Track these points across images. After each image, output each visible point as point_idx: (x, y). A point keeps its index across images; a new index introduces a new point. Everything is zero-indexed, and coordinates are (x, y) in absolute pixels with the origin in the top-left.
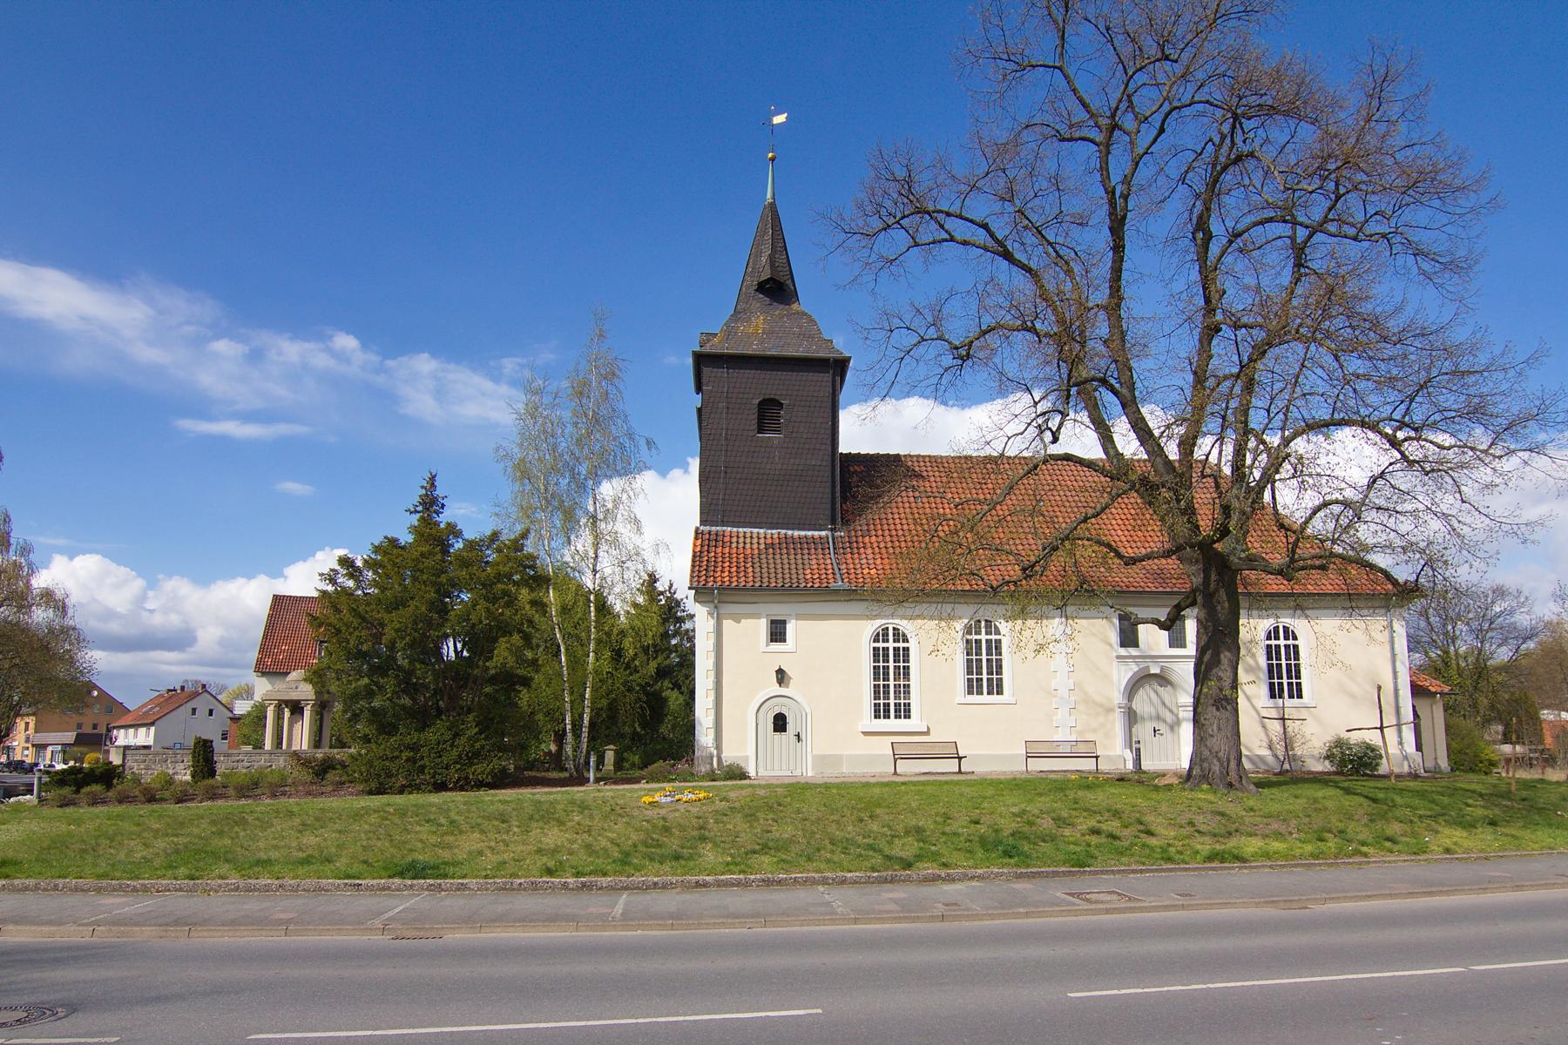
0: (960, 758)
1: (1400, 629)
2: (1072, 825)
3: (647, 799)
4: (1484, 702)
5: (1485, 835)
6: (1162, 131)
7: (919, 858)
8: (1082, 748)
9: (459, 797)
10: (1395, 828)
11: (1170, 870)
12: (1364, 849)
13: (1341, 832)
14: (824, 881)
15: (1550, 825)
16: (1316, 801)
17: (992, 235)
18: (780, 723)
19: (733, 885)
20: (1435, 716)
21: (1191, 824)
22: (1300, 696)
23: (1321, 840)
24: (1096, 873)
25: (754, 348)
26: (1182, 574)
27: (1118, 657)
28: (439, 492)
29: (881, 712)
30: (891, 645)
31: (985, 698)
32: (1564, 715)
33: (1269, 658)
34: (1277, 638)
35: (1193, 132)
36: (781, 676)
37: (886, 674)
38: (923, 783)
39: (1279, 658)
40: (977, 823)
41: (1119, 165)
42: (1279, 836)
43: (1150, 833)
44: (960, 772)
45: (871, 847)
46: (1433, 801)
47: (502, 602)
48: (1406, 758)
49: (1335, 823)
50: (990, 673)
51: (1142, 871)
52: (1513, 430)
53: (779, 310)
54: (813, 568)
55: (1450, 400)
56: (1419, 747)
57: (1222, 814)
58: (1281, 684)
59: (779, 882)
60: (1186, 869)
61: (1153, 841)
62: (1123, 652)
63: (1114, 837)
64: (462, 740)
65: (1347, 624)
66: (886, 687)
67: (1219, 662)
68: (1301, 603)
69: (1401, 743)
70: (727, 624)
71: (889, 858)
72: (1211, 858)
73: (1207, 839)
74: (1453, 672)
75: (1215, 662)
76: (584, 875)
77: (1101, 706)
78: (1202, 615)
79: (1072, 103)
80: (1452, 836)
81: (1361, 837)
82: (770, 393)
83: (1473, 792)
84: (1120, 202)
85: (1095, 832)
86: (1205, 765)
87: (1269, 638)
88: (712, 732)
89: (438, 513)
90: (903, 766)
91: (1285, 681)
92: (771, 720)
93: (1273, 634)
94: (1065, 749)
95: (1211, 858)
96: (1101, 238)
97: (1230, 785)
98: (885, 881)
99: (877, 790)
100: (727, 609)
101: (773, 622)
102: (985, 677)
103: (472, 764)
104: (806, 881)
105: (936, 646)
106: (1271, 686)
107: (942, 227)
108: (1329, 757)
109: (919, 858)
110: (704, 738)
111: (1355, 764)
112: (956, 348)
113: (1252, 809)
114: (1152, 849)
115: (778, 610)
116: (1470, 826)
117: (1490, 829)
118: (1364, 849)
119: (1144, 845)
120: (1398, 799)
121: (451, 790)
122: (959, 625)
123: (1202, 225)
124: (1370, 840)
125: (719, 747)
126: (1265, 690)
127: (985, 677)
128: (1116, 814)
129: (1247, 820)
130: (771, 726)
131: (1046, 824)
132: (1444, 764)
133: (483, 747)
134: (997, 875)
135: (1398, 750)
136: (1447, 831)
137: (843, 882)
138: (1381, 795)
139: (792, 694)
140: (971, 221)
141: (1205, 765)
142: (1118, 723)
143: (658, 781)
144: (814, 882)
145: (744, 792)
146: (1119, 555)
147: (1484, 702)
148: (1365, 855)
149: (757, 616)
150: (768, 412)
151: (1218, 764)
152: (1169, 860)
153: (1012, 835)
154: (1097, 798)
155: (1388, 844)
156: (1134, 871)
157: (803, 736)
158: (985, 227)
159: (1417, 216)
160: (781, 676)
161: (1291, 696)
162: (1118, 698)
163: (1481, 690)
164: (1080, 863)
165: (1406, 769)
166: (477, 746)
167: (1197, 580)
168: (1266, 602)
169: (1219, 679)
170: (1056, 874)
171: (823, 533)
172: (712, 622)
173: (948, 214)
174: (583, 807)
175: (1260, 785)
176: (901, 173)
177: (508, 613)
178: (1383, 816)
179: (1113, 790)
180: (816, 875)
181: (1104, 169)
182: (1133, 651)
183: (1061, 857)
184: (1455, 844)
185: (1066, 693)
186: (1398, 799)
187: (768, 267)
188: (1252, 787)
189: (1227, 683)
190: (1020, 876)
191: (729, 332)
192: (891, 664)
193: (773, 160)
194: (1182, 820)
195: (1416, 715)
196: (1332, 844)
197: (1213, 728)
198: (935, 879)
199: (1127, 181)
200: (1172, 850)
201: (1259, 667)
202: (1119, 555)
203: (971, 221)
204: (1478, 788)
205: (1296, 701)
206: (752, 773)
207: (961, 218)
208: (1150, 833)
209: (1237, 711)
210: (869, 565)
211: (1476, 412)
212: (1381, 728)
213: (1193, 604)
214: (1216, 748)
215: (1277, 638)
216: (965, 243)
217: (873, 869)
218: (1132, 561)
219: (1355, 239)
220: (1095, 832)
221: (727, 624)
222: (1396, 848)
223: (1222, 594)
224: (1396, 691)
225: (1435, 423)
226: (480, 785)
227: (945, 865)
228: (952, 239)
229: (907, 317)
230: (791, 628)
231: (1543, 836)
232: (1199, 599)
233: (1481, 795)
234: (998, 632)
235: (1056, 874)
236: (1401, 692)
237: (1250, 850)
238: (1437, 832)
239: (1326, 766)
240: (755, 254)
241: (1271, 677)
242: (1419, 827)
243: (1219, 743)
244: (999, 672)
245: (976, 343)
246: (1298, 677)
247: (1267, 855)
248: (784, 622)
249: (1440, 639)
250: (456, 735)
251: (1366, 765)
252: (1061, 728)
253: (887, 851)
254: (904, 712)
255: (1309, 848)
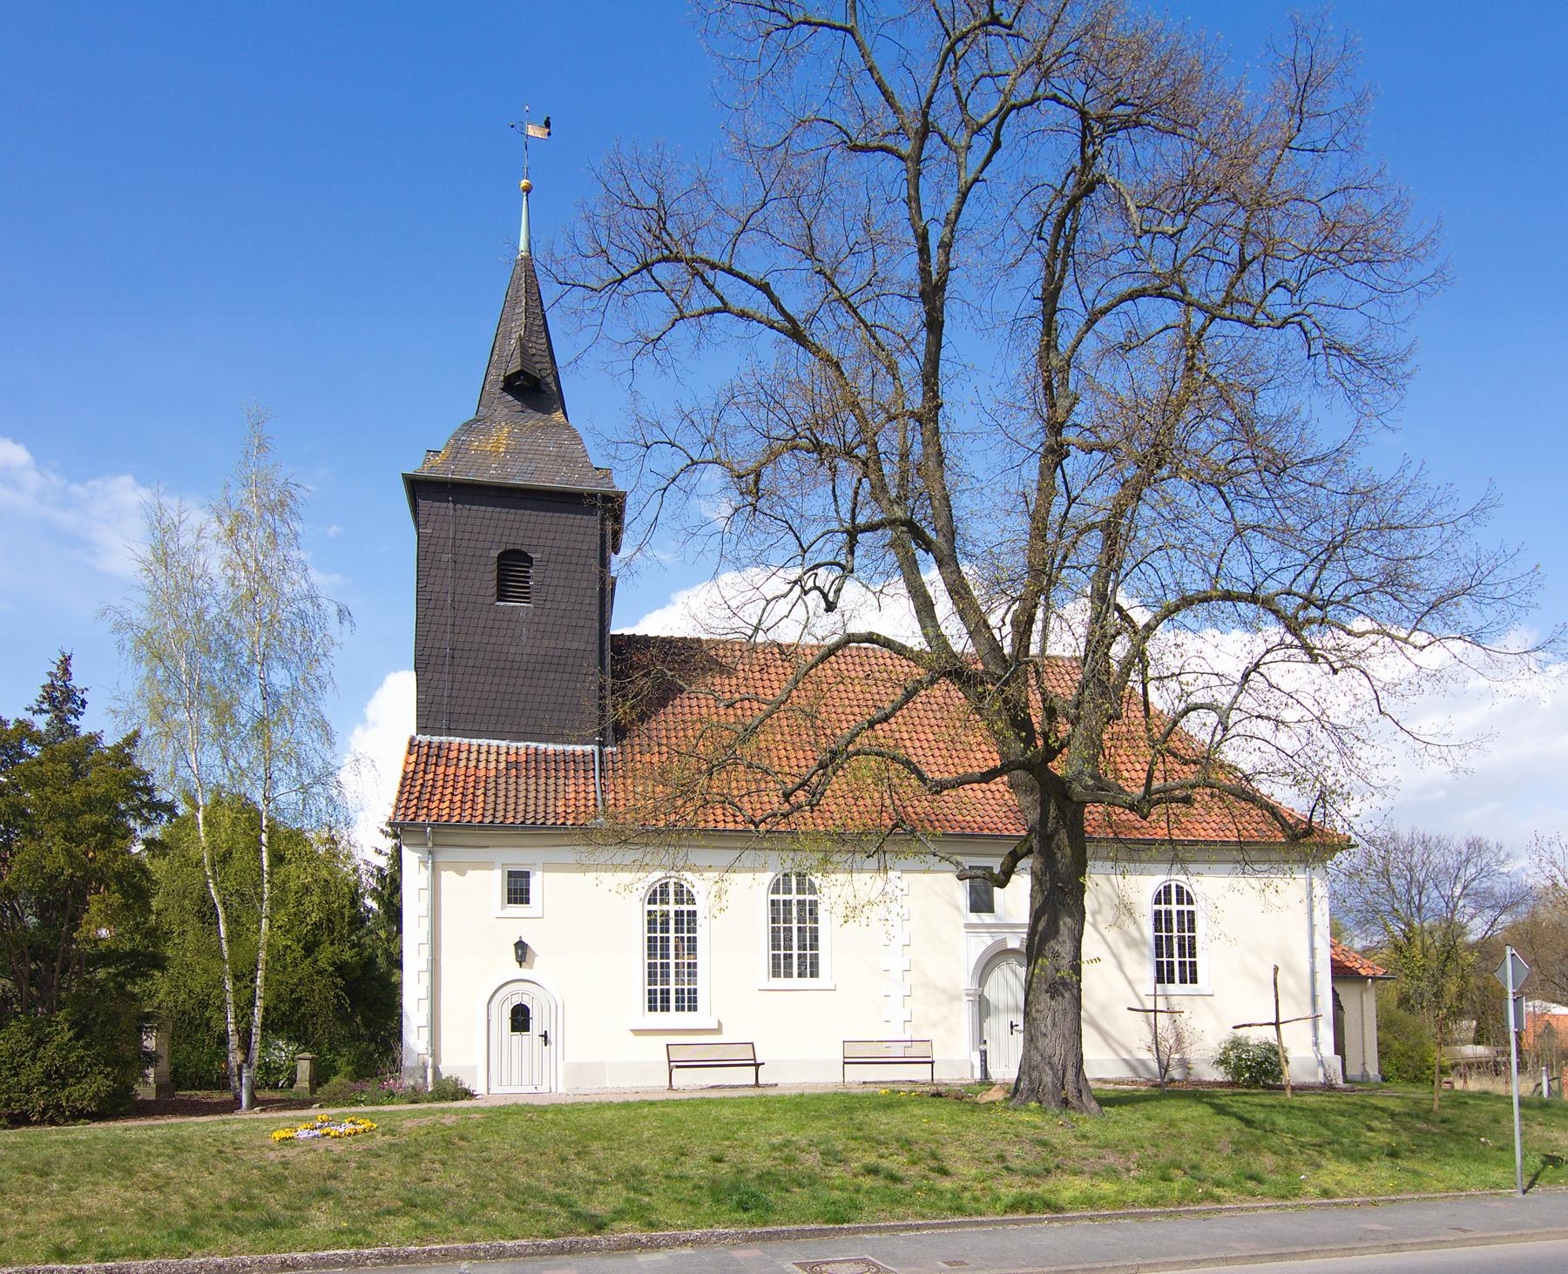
0: (757, 1065)
1: (1320, 890)
2: (845, 1161)
3: (278, 1135)
4: (1452, 987)
5: (1381, 1170)
6: (997, 145)
7: (620, 1214)
8: (917, 1051)
9: (52, 1133)
10: (1267, 1161)
11: (957, 1225)
12: (1218, 1191)
13: (1194, 1167)
14: (473, 1255)
15: (1465, 1157)
16: (1172, 1123)
17: (775, 302)
18: (520, 1019)
19: (337, 1264)
20: (1364, 1009)
21: (1001, 1158)
22: (1194, 980)
23: (1165, 1178)
24: (856, 1231)
25: (491, 474)
26: (998, 806)
27: (968, 926)
28: (77, 682)
29: (658, 1001)
30: (672, 908)
31: (795, 982)
32: (1558, 1010)
33: (1157, 929)
34: (1168, 902)
35: (1043, 153)
36: (522, 951)
37: (665, 948)
38: (721, 1102)
39: (1169, 929)
40: (720, 1160)
41: (937, 201)
42: (1112, 1174)
43: (944, 1172)
44: (757, 1085)
45: (558, 1201)
46: (1325, 1125)
47: (93, 841)
48: (1321, 1063)
49: (1189, 1156)
50: (802, 947)
51: (918, 1227)
52: (1421, 601)
53: (534, 419)
54: (575, 795)
55: (1367, 567)
56: (1339, 1048)
57: (1044, 1144)
58: (1170, 964)
59: (407, 1258)
60: (977, 1224)
61: (946, 1184)
62: (974, 918)
63: (893, 1178)
64: (51, 1049)
65: (1242, 882)
66: (665, 966)
67: (1057, 932)
68: (1179, 852)
69: (1316, 1044)
70: (447, 877)
71: (577, 1216)
72: (1013, 1207)
73: (1017, 1180)
74: (1417, 952)
75: (1052, 931)
76: (112, 1257)
77: (944, 991)
78: (1038, 866)
79: (872, 96)
80: (1337, 1172)
81: (1217, 1174)
82: (515, 541)
83: (1383, 1110)
84: (936, 256)
85: (872, 1171)
86: (1035, 1074)
87: (1158, 901)
88: (425, 1033)
89: (77, 714)
90: (683, 1078)
91: (1176, 960)
92: (507, 1015)
93: (1163, 896)
94: (897, 1051)
95: (1013, 1207)
96: (911, 315)
97: (1065, 1102)
98: (561, 1251)
99: (608, 1114)
100: (445, 855)
101: (511, 874)
102: (795, 952)
103: (65, 1085)
104: (446, 1254)
105: (734, 904)
106: (1159, 965)
107: (711, 287)
108: (1223, 1061)
109: (620, 1214)
110: (415, 1039)
111: (1257, 1070)
112: (740, 477)
113: (1084, 1137)
114: (941, 1194)
115: (518, 858)
116: (1359, 1157)
117: (1388, 1162)
118: (1218, 1191)
119: (932, 1189)
120: (1281, 1121)
121: (36, 1123)
122: (767, 878)
123: (1050, 300)
124: (1229, 1179)
125: (435, 1053)
126: (1150, 972)
127: (795, 952)
128: (907, 1144)
129: (1075, 1151)
130: (508, 1024)
131: (811, 1160)
132: (1373, 1071)
133: (81, 1059)
134: (721, 1237)
135: (1306, 1052)
136: (1332, 1166)
137: (500, 1254)
138: (1260, 1115)
139: (538, 981)
140: (745, 279)
141: (1035, 1074)
142: (964, 1014)
143: (336, 1105)
144: (458, 1256)
145: (426, 1121)
146: (921, 777)
147: (1452, 987)
148: (1218, 1200)
149: (488, 866)
150: (512, 570)
151: (1053, 1080)
152: (959, 1209)
153: (760, 1177)
154: (887, 1123)
155: (1251, 1184)
156: (909, 1228)
157: (552, 1037)
158: (765, 288)
159: (1327, 288)
160: (522, 951)
161: (1183, 981)
162: (965, 980)
163: (1431, 978)
164: (838, 1217)
165: (1321, 1078)
166: (73, 1057)
167: (1034, 816)
168: (1132, 850)
169: (1056, 955)
170: (801, 1234)
171: (588, 748)
172: (426, 874)
173: (713, 267)
174: (179, 1148)
175: (1105, 1102)
176: (650, 201)
177: (101, 857)
178: (1254, 1146)
179: (917, 1111)
180: (461, 1245)
181: (913, 201)
182: (986, 918)
183: (816, 1207)
184: (1338, 1183)
185: (893, 976)
186: (1281, 1121)
187: (517, 354)
188: (1094, 1105)
189: (1066, 961)
190: (750, 1238)
191: (458, 448)
192: (672, 935)
193: (528, 190)
194: (991, 1153)
195: (1338, 1006)
196: (1180, 1183)
197: (1046, 1025)
198: (634, 1245)
199: (952, 222)
200: (967, 1194)
201: (1144, 942)
202: (921, 777)
203: (745, 279)
204: (1393, 1105)
205: (1188, 987)
206: (479, 1087)
207: (730, 271)
208: (944, 1172)
209: (1079, 999)
210: (635, 793)
211: (1393, 582)
212: (1277, 1024)
213: (1030, 851)
214: (1049, 1052)
215: (1168, 902)
216: (742, 315)
217: (549, 1234)
218: (940, 787)
219: (1251, 323)
220: (872, 1171)
221: (447, 877)
222: (1264, 1188)
223: (1063, 836)
224: (1313, 973)
225: (1347, 599)
226: (79, 1115)
227: (651, 1225)
228: (725, 309)
229: (671, 426)
230: (536, 883)
231: (1453, 1172)
232: (1035, 843)
233: (1392, 1115)
234: (813, 890)
235: (801, 1234)
236: (1318, 976)
237: (1068, 1194)
238: (1319, 1167)
239: (1217, 1075)
240: (501, 335)
241: (1159, 954)
242: (1297, 1161)
243: (1053, 1045)
244: (814, 947)
245: (767, 473)
246: (1192, 955)
247: (1090, 1202)
248: (527, 875)
249: (1401, 906)
250: (40, 1043)
251: (1266, 1073)
252: (883, 1023)
253: (581, 1206)
254: (688, 1002)
255: (1147, 1190)
